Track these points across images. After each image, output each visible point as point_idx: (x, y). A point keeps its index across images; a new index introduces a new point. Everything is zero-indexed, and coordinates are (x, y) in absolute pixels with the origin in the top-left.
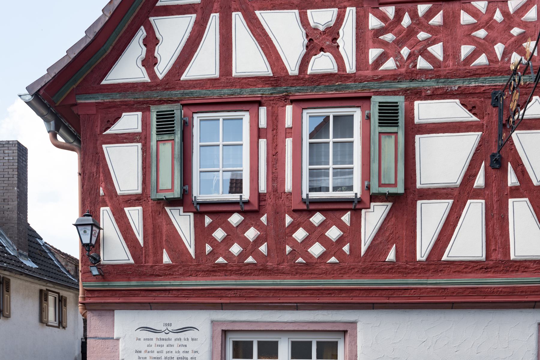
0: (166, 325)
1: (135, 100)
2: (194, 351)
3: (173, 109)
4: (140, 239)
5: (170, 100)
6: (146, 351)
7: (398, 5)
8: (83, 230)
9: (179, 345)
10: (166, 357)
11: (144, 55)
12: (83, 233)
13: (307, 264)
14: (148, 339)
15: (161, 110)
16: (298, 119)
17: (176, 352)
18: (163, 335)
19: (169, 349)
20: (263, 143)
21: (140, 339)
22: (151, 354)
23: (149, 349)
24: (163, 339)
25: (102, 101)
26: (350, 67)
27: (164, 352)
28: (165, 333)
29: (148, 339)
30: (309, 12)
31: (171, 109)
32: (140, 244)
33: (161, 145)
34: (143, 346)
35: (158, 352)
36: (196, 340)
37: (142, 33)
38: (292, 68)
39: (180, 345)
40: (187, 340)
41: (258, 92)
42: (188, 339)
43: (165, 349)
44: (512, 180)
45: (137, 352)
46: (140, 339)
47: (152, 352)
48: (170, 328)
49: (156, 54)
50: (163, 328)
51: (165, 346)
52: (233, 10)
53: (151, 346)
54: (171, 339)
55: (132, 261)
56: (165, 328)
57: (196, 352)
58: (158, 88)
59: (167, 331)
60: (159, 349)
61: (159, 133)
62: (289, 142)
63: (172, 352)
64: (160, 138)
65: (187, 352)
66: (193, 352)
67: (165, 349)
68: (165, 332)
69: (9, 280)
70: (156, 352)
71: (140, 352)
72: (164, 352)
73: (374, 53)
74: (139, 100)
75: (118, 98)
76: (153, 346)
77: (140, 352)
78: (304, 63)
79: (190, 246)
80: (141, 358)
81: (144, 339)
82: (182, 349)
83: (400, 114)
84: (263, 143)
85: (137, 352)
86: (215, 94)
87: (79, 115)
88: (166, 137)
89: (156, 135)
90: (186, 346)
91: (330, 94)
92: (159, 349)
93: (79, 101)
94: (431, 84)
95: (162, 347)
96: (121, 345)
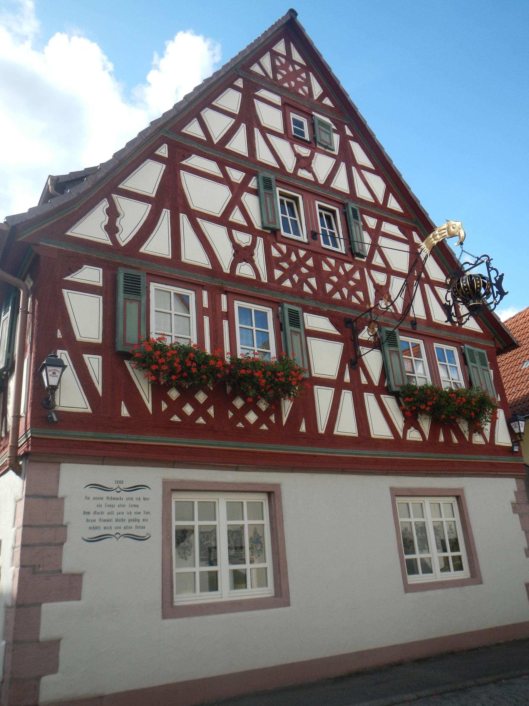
0: (117, 482)
1: (97, 257)
2: (145, 512)
3: (139, 275)
4: (99, 388)
5: (129, 266)
6: (95, 513)
7: (289, 246)
8: (53, 371)
9: (131, 505)
10: (117, 519)
11: (106, 222)
12: (52, 374)
13: (245, 429)
14: (98, 499)
15: (128, 272)
16: (230, 306)
17: (128, 513)
18: (113, 494)
19: (121, 509)
20: (206, 320)
21: (89, 498)
22: (100, 516)
23: (99, 510)
24: (114, 499)
25: (66, 249)
26: (264, 279)
27: (116, 513)
28: (116, 491)
29: (98, 499)
30: (384, 223)
31: (138, 274)
32: (467, 440)
33: (128, 304)
34: (92, 506)
35: (108, 513)
36: (148, 499)
37: (104, 204)
38: (226, 268)
39: (131, 506)
40: (138, 499)
41: (200, 279)
42: (140, 499)
43: (116, 510)
44: (364, 381)
45: (85, 513)
46: (89, 498)
47: (102, 513)
48: (122, 486)
49: (117, 224)
50: (115, 486)
51: (116, 506)
52: (180, 211)
53: (101, 506)
54: (122, 498)
55: (89, 410)
56: (116, 486)
57: (148, 513)
58: (120, 253)
59: (118, 490)
60: (110, 509)
61: (126, 291)
62: (225, 323)
63: (123, 513)
64: (127, 296)
65: (139, 513)
66: (145, 513)
67: (116, 510)
68: (117, 490)
69: (278, 486)
70: (106, 513)
71: (89, 513)
72: (116, 513)
73: (278, 274)
74: (100, 257)
75: (81, 251)
76: (103, 506)
77: (89, 513)
78: (233, 267)
79: (149, 401)
80: (90, 521)
81: (94, 498)
82: (133, 510)
83: (288, 319)
84: (206, 320)
85: (85, 513)
86: (166, 271)
87: (40, 256)
88: (132, 297)
89: (123, 293)
90: (138, 506)
91: (250, 293)
92: (110, 509)
93: (42, 243)
94: (312, 304)
95: (112, 507)
96: (67, 506)
